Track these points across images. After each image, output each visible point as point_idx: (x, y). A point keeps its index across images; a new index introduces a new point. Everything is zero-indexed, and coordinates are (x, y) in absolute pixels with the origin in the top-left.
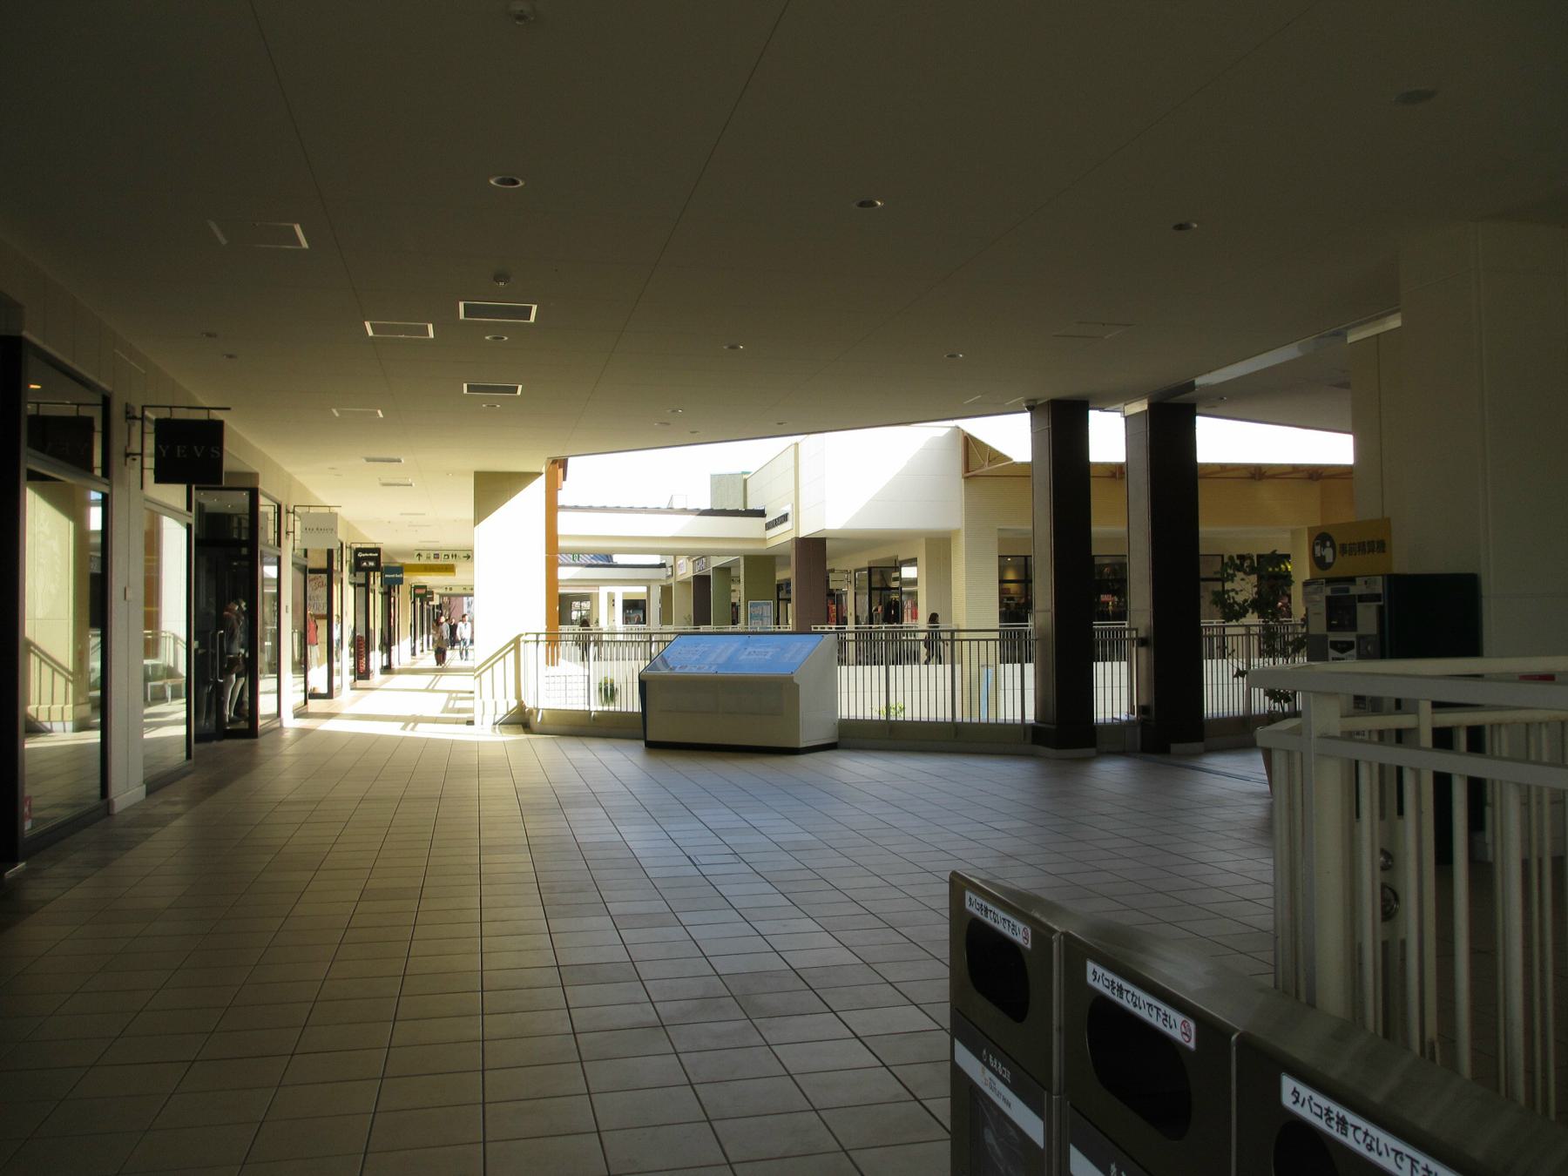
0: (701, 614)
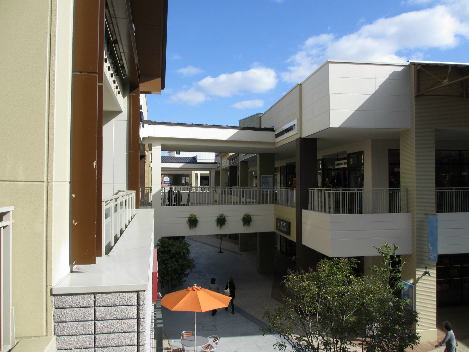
0: (233, 182)
